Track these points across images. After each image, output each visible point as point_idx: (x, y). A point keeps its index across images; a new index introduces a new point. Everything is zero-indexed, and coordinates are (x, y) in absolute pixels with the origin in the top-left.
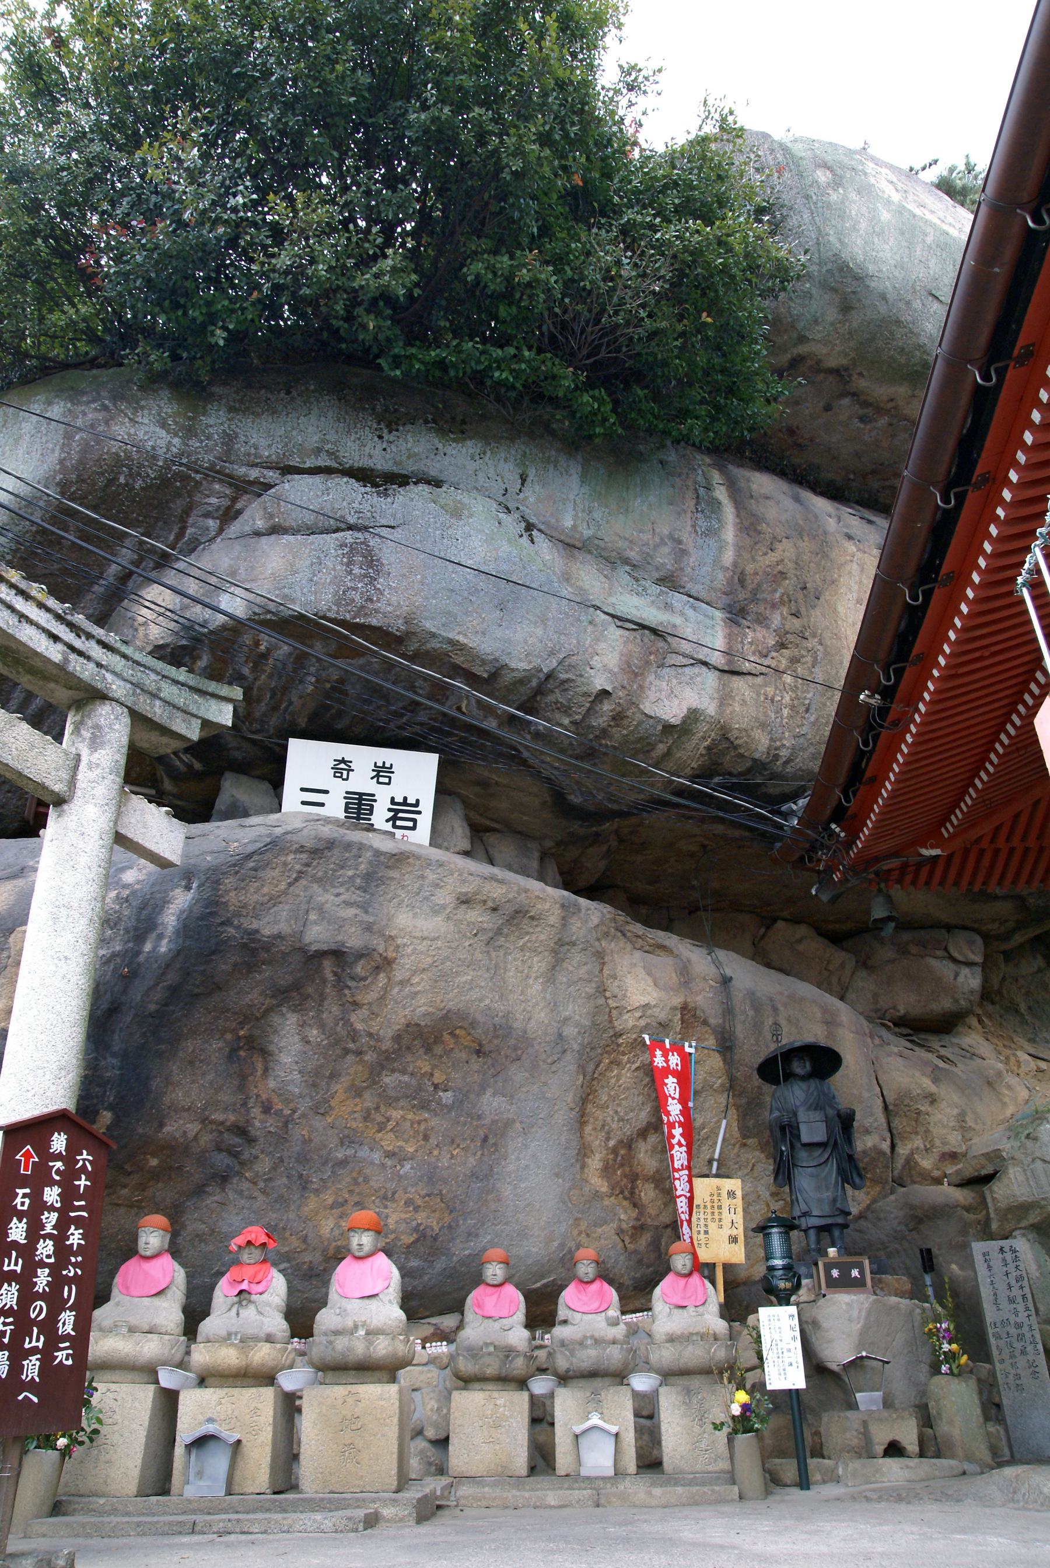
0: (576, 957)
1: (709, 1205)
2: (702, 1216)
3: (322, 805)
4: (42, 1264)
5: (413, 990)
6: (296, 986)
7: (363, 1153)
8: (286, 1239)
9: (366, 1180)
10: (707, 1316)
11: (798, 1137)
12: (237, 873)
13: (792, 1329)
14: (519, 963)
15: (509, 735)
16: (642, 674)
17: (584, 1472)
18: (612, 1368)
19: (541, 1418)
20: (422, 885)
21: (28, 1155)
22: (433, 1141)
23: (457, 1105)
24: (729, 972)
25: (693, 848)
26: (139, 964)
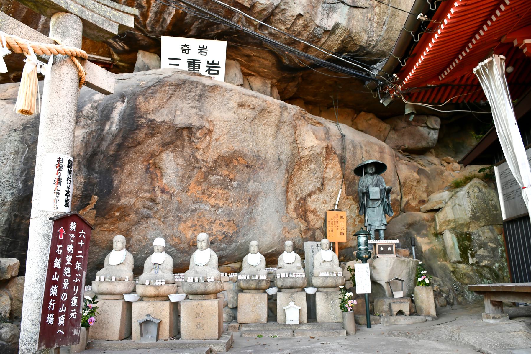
1: (333, 221)
2: (331, 225)
3: (178, 65)
4: (66, 278)
5: (221, 142)
6: (172, 142)
7: (203, 206)
8: (173, 239)
9: (204, 216)
12: (144, 95)
15: (258, 33)
16: (316, 7)
17: (288, 323)
18: (298, 285)
19: (272, 299)
20: (224, 99)
21: (61, 231)
22: (230, 201)
23: (239, 186)
24: (344, 133)
25: (331, 83)
26: (104, 135)
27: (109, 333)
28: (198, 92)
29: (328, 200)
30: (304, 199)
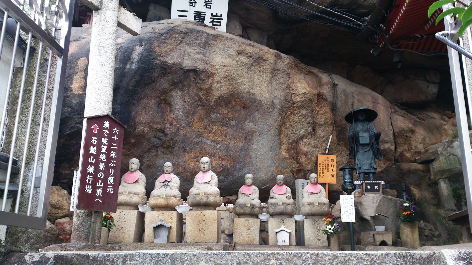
0: (280, 75)
1: (324, 164)
2: (321, 168)
3: (186, 16)
6: (180, 82)
7: (204, 140)
8: (178, 168)
9: (205, 150)
10: (322, 198)
11: (359, 141)
13: (351, 202)
14: (259, 76)
19: (264, 229)
21: (95, 127)
22: (228, 137)
24: (336, 82)
26: (125, 72)
27: (125, 236)
28: (203, 40)
29: (319, 145)
30: (297, 142)
